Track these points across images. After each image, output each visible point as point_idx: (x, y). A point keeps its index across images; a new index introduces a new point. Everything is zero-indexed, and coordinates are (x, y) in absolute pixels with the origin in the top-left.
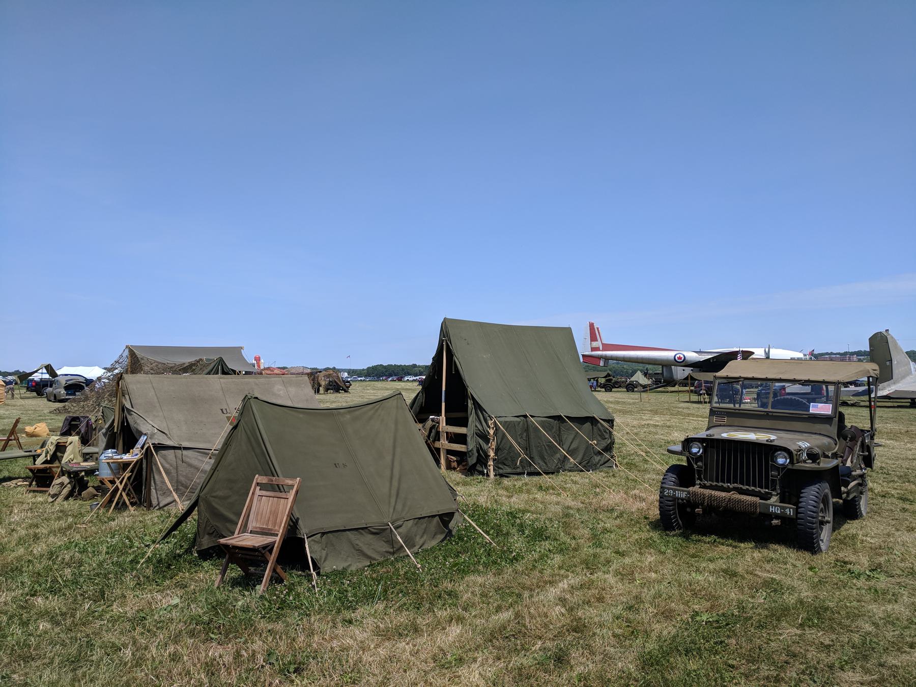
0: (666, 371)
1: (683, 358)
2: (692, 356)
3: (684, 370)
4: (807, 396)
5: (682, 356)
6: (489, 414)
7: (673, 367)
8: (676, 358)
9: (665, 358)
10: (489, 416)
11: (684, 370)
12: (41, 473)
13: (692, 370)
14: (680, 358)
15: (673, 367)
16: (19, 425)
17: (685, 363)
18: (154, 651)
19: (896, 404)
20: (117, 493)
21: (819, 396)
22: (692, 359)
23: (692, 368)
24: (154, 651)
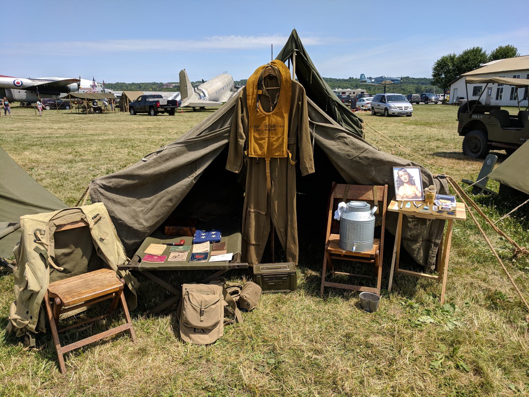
0: (8, 92)
1: (21, 83)
2: (27, 82)
3: (19, 92)
4: (165, 107)
5: (19, 82)
6: (358, 117)
7: (12, 89)
8: (15, 83)
9: (6, 83)
10: (359, 119)
11: (19, 92)
12: (377, 275)
13: (26, 92)
14: (18, 83)
15: (12, 89)
16: (57, 370)
17: (21, 87)
18: (502, 223)
19: (185, 111)
20: (323, 262)
21: (175, 106)
22: (28, 84)
23: (26, 91)
24: (502, 223)
